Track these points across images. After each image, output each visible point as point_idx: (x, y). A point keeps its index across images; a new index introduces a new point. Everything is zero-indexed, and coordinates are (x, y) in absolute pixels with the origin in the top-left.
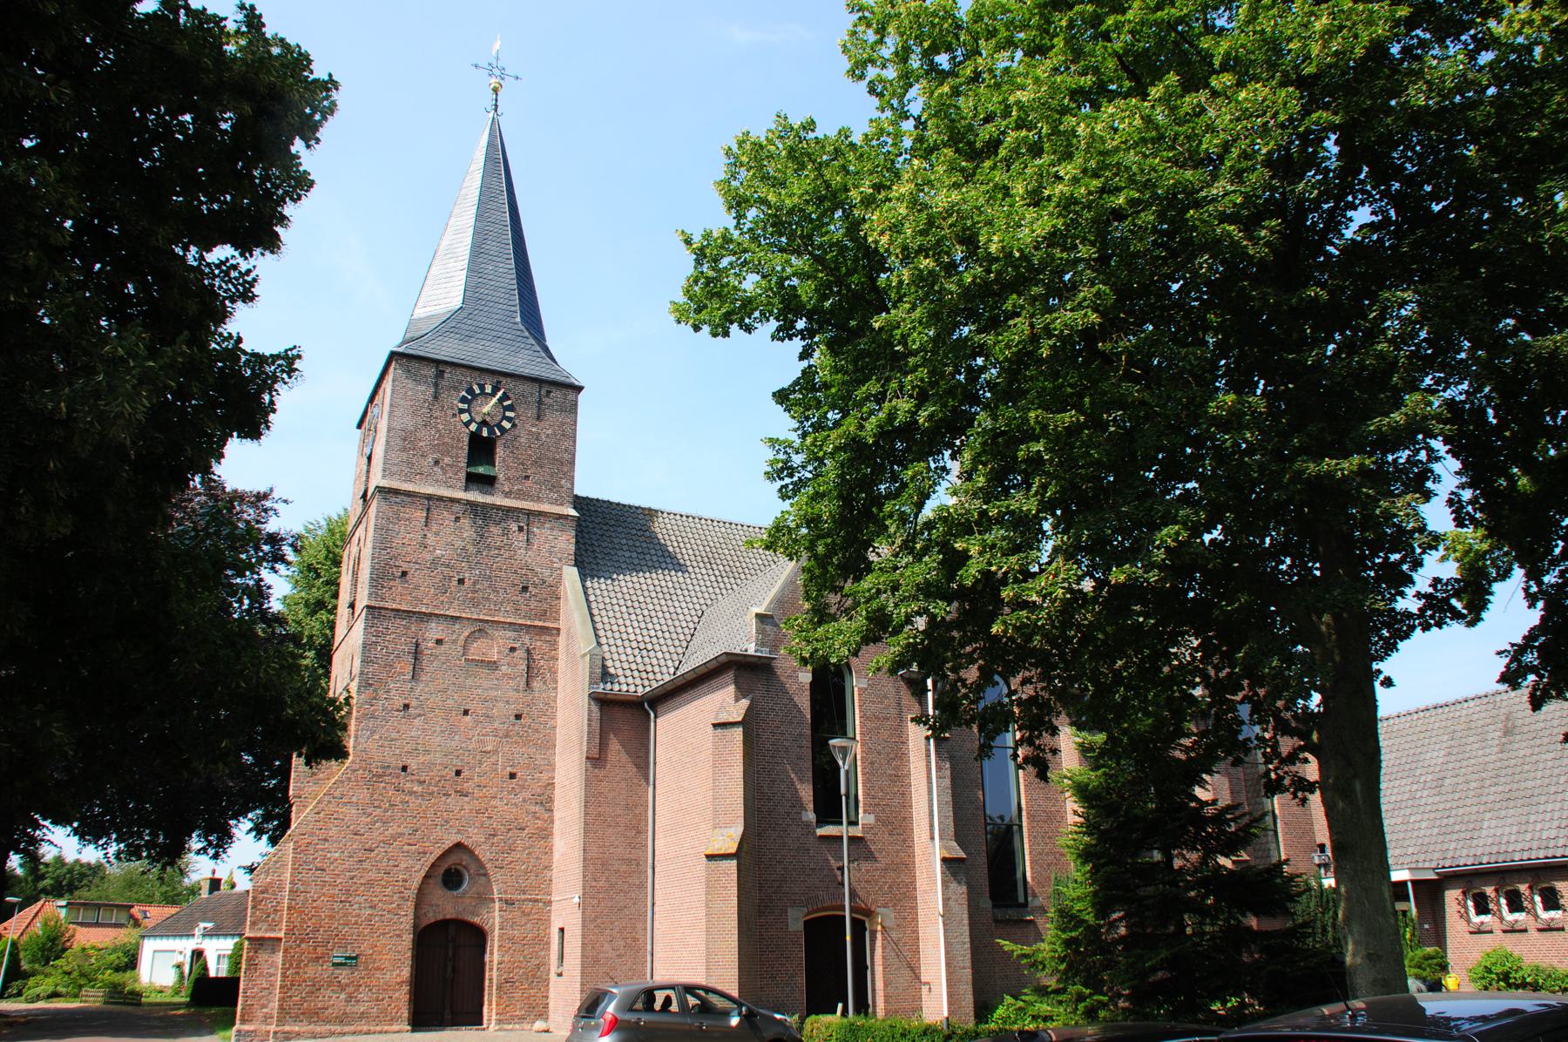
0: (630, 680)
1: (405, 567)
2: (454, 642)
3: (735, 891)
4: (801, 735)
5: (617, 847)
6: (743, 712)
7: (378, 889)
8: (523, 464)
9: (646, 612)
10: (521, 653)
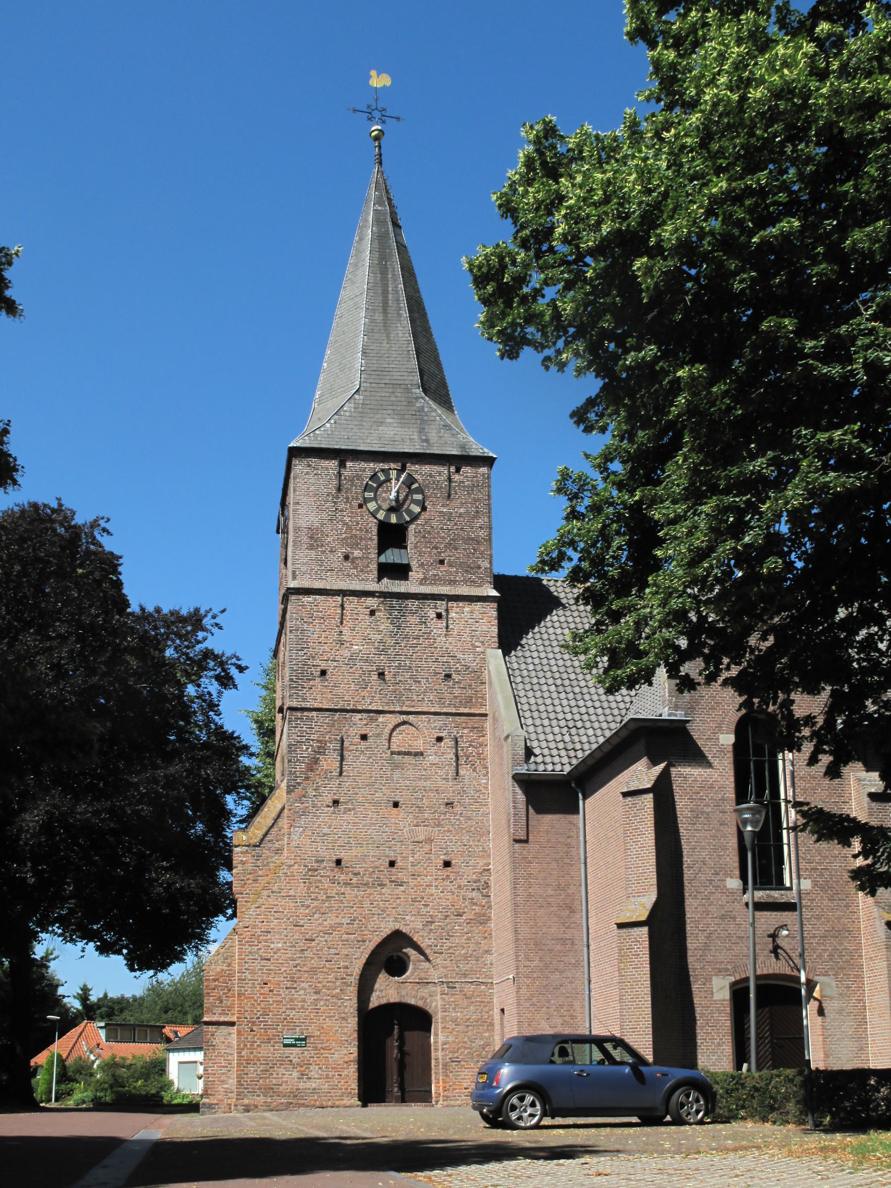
0: (557, 759)
1: (323, 665)
2: (378, 735)
3: (646, 958)
4: (723, 799)
5: (550, 927)
6: (654, 778)
7: (321, 976)
8: (436, 548)
9: (577, 690)
10: (448, 743)
